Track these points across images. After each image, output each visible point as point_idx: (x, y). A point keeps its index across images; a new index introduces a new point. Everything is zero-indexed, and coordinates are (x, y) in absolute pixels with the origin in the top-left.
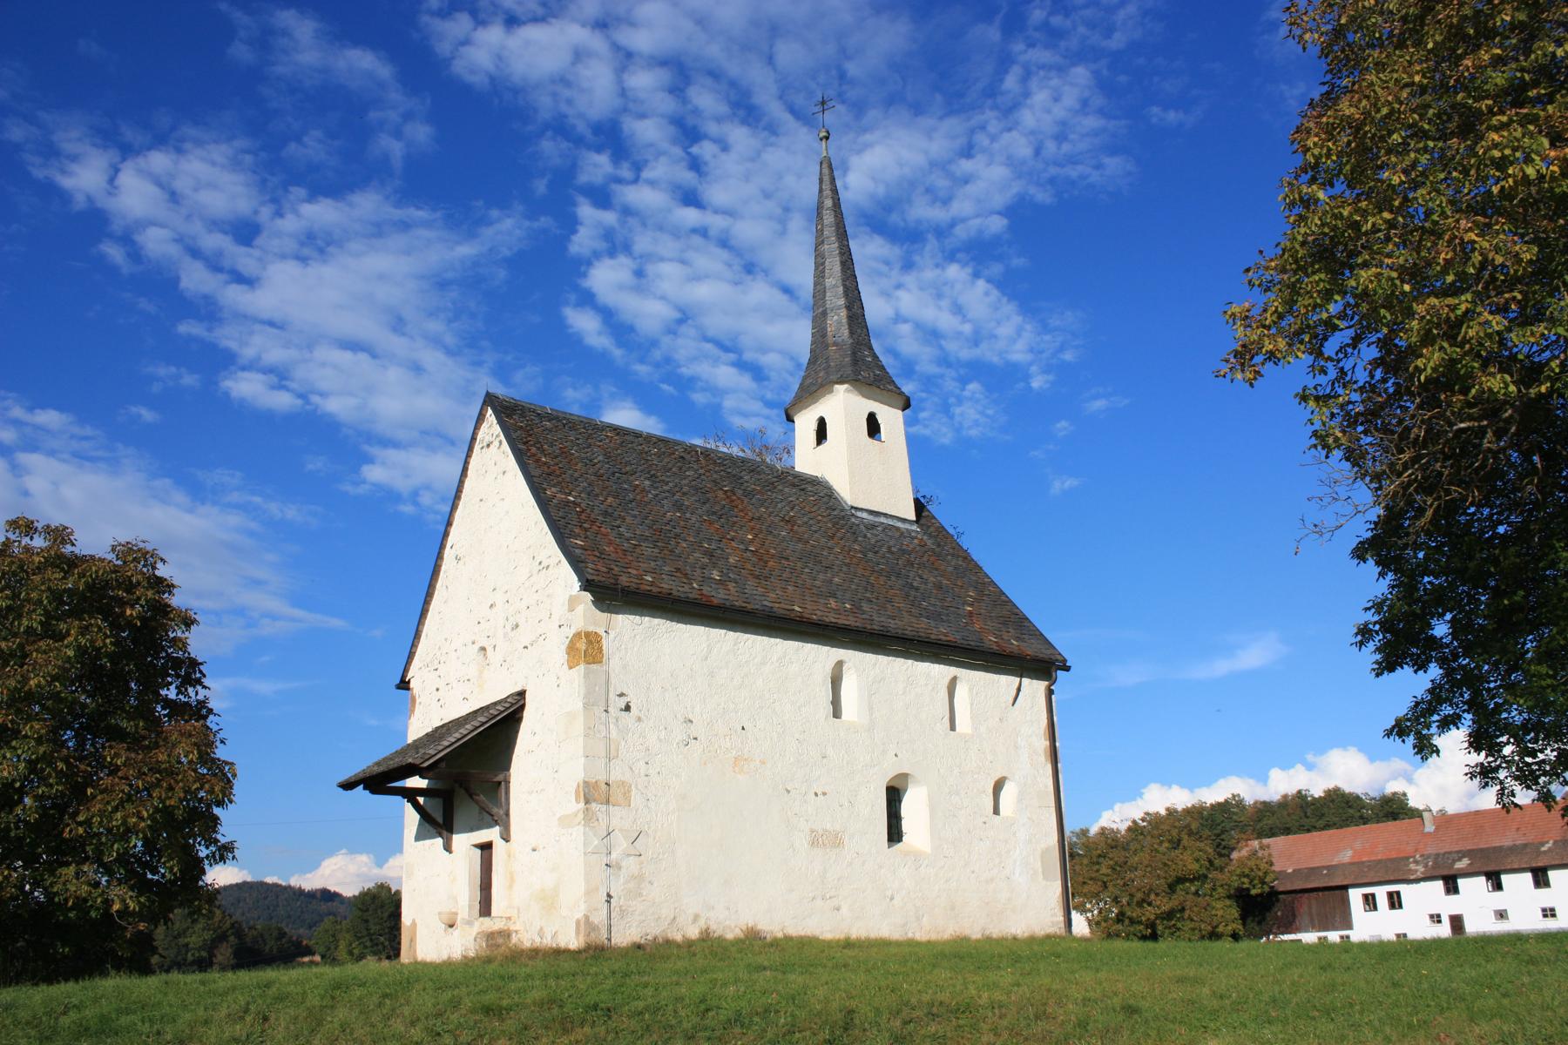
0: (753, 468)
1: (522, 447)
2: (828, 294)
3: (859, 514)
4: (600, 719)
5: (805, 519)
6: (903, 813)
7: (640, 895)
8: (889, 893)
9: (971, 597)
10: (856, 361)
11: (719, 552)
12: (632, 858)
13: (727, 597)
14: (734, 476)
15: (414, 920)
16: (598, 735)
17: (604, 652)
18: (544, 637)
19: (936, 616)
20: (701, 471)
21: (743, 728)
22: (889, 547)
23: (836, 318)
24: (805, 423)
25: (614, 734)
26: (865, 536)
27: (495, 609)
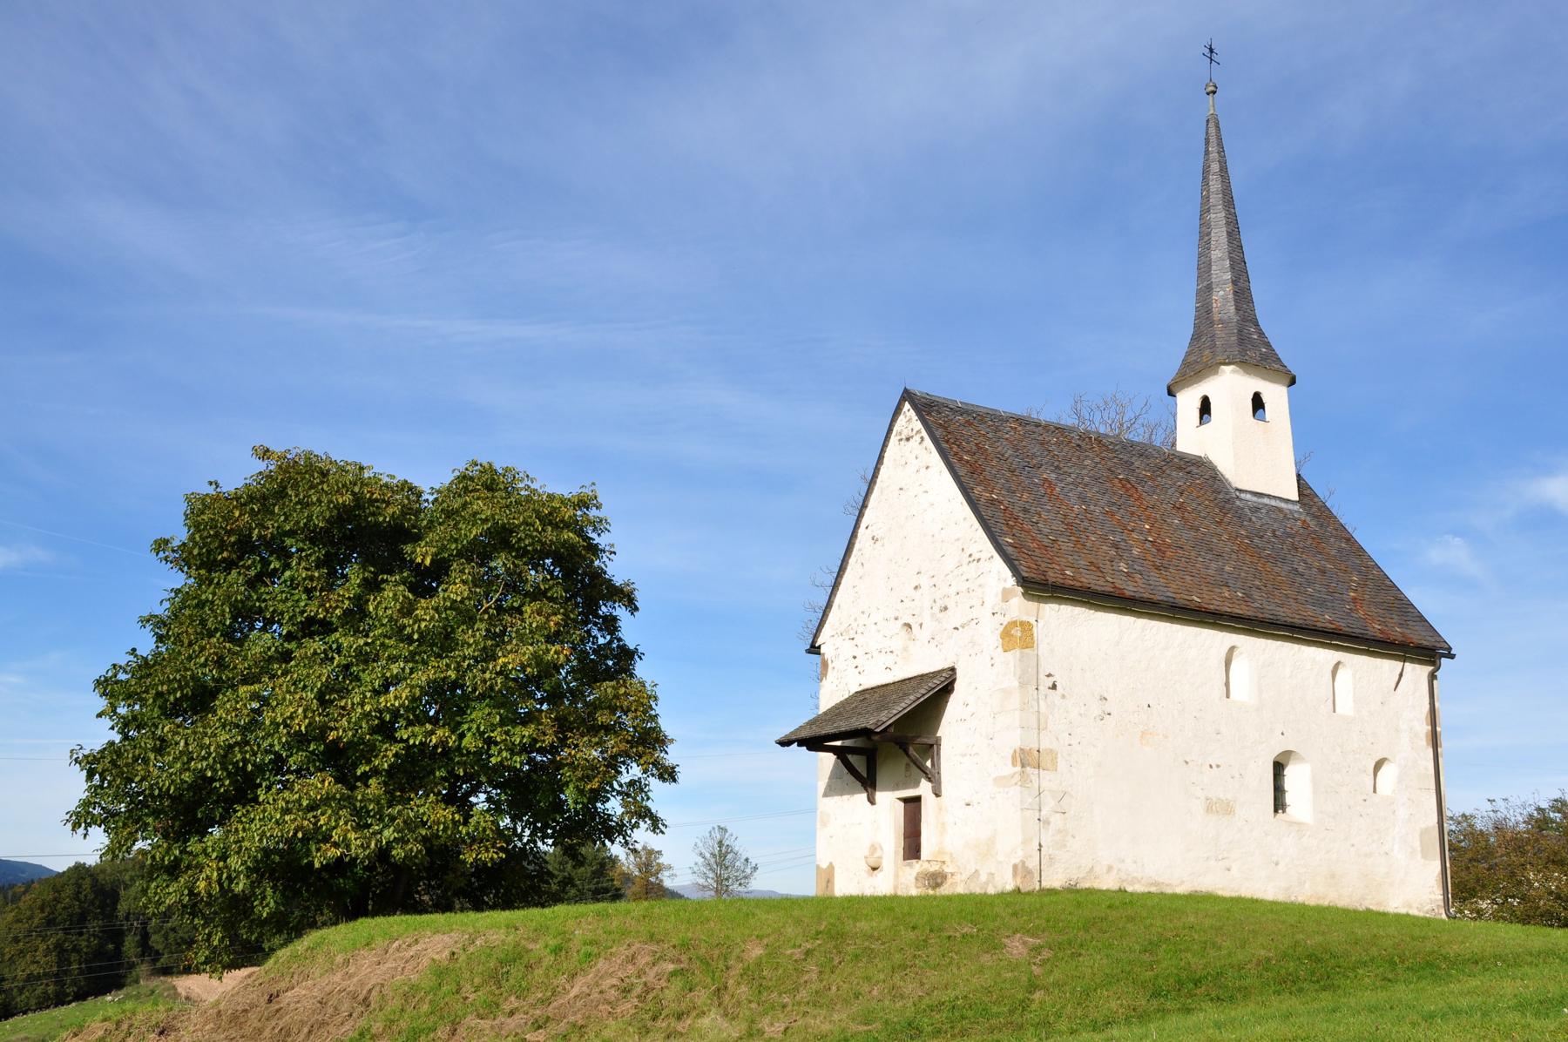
0: (1143, 451)
1: (945, 445)
2: (1214, 267)
5: (1194, 505)
7: (1065, 846)
8: (1275, 859)
10: (1243, 339)
14: (1126, 462)
15: (831, 863)
16: (1031, 710)
17: (1036, 639)
19: (1322, 603)
20: (1097, 460)
21: (1149, 706)
22: (1274, 531)
23: (1222, 293)
24: (1188, 401)
26: (1250, 519)
27: (919, 592)
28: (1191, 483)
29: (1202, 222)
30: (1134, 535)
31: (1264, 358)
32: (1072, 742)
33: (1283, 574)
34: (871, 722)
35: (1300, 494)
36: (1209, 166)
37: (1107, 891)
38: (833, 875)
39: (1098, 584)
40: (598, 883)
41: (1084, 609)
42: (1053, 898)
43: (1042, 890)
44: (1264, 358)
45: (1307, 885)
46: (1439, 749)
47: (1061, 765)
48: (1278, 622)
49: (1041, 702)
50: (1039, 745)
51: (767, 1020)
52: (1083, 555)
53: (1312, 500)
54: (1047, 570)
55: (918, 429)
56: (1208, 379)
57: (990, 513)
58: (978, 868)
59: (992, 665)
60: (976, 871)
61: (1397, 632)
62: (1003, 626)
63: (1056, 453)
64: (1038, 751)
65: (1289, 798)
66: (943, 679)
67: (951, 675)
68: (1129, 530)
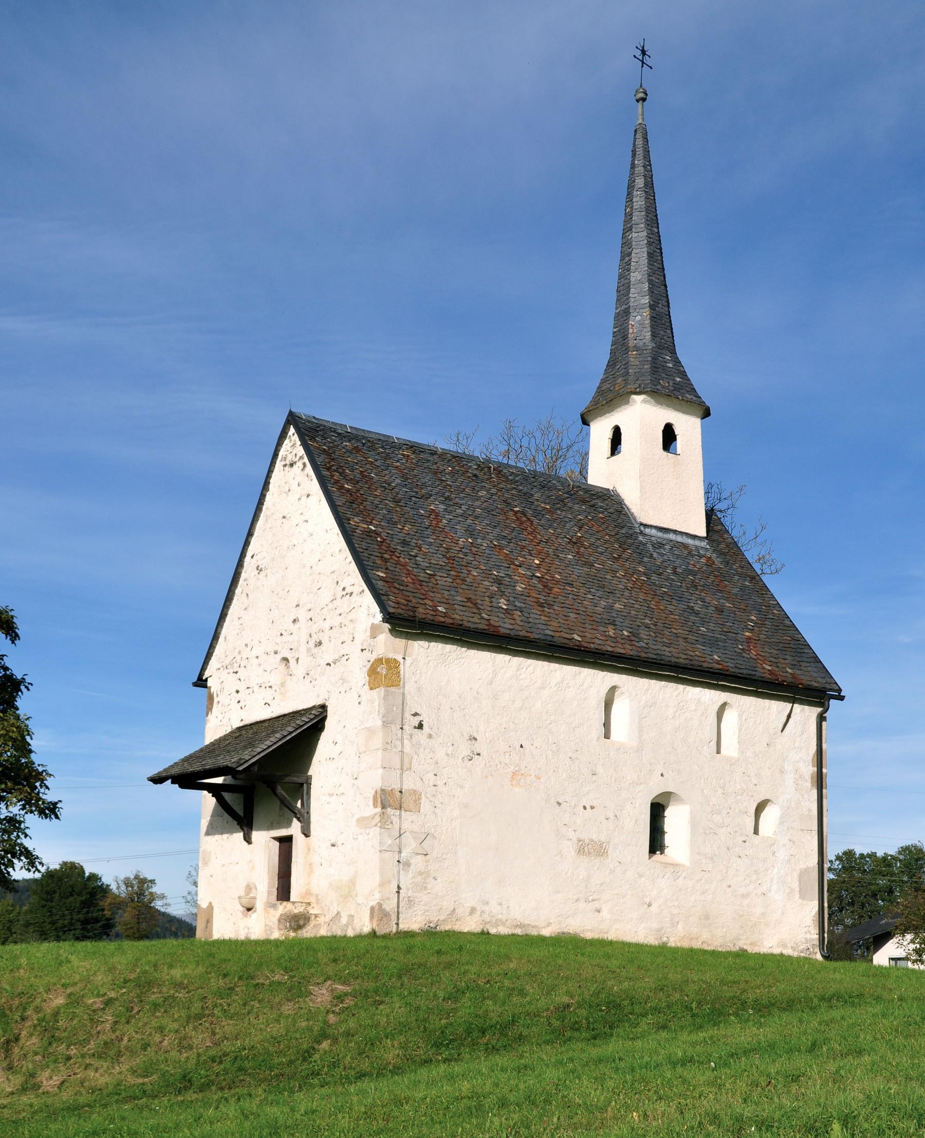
1: (325, 473)
2: (632, 290)
3: (647, 531)
4: (397, 735)
6: (667, 828)
7: (426, 888)
8: (647, 900)
9: (752, 621)
10: (657, 367)
11: (507, 579)
12: (419, 856)
13: (511, 627)
15: (210, 903)
16: (395, 750)
17: (402, 677)
18: (346, 657)
19: (712, 643)
20: (494, 491)
21: (521, 746)
22: (674, 569)
23: (639, 318)
24: (600, 431)
25: (407, 749)
26: (651, 556)
27: (298, 625)
28: (593, 517)
29: (624, 241)
30: (521, 571)
31: (678, 388)
32: (438, 783)
33: (677, 612)
34: (233, 760)
35: (708, 530)
36: (634, 181)
37: (469, 933)
38: (212, 914)
39: (472, 621)
40: (88, 912)
41: (455, 647)
42: (408, 941)
43: (398, 933)
44: (678, 388)
45: (680, 926)
46: (824, 791)
47: (425, 806)
48: (662, 662)
49: (406, 742)
50: (402, 785)
51: (47, 1073)
52: (461, 591)
53: (722, 537)
54: (418, 605)
55: (301, 455)
56: (619, 409)
57: (364, 545)
58: (339, 909)
59: (359, 703)
60: (338, 913)
61: (788, 672)
62: (371, 663)
63: (449, 483)
64: (401, 792)
65: (668, 839)
66: (312, 716)
67: (322, 713)
68: (517, 566)
